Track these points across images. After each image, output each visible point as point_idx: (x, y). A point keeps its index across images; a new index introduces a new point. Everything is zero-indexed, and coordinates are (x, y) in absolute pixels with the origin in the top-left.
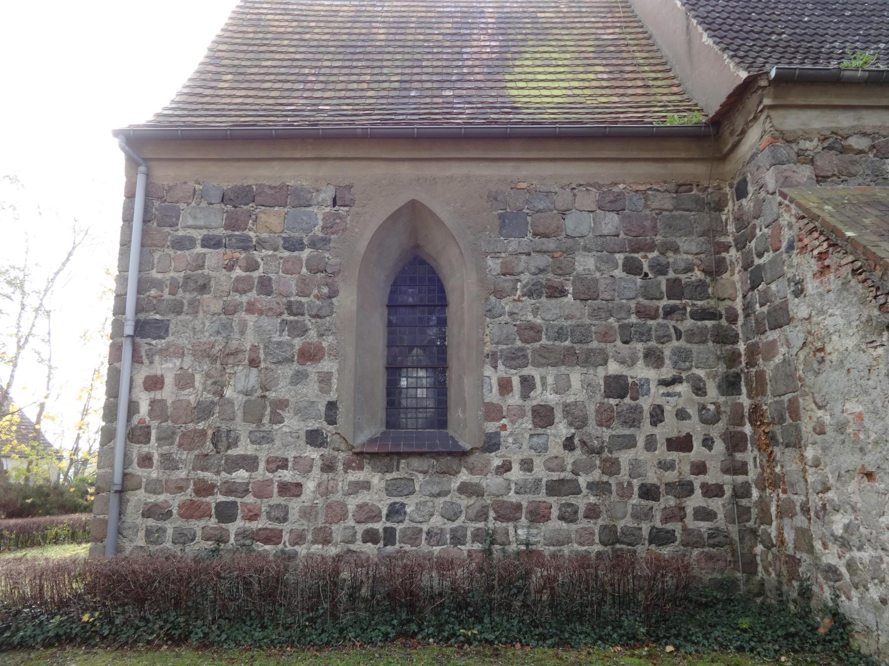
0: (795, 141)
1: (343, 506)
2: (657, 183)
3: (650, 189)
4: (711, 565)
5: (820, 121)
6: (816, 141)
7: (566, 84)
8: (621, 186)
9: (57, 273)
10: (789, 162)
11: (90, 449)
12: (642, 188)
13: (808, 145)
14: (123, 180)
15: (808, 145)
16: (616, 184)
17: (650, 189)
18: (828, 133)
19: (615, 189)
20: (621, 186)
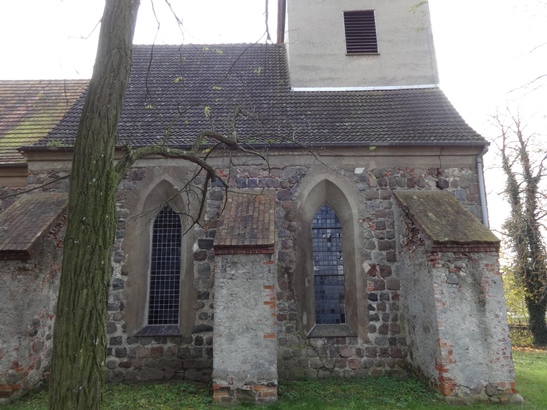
0: (37, 174)
1: (191, 337)
2: (22, 186)
3: (19, 189)
4: (503, 332)
5: (47, 166)
6: (46, 174)
7: (39, 131)
8: (7, 188)
9: (267, 30)
10: (33, 183)
11: (503, 131)
12: (16, 188)
13: (42, 176)
14: (86, 79)
15: (42, 176)
16: (4, 187)
17: (19, 189)
18: (51, 171)
19: (4, 190)
20: (7, 188)
